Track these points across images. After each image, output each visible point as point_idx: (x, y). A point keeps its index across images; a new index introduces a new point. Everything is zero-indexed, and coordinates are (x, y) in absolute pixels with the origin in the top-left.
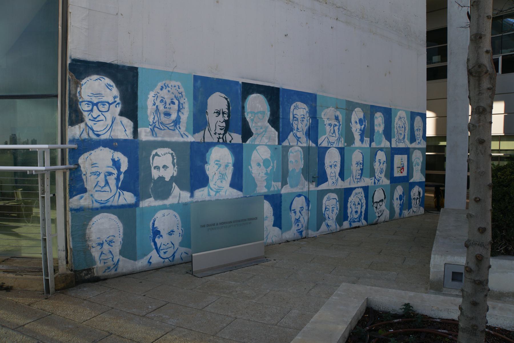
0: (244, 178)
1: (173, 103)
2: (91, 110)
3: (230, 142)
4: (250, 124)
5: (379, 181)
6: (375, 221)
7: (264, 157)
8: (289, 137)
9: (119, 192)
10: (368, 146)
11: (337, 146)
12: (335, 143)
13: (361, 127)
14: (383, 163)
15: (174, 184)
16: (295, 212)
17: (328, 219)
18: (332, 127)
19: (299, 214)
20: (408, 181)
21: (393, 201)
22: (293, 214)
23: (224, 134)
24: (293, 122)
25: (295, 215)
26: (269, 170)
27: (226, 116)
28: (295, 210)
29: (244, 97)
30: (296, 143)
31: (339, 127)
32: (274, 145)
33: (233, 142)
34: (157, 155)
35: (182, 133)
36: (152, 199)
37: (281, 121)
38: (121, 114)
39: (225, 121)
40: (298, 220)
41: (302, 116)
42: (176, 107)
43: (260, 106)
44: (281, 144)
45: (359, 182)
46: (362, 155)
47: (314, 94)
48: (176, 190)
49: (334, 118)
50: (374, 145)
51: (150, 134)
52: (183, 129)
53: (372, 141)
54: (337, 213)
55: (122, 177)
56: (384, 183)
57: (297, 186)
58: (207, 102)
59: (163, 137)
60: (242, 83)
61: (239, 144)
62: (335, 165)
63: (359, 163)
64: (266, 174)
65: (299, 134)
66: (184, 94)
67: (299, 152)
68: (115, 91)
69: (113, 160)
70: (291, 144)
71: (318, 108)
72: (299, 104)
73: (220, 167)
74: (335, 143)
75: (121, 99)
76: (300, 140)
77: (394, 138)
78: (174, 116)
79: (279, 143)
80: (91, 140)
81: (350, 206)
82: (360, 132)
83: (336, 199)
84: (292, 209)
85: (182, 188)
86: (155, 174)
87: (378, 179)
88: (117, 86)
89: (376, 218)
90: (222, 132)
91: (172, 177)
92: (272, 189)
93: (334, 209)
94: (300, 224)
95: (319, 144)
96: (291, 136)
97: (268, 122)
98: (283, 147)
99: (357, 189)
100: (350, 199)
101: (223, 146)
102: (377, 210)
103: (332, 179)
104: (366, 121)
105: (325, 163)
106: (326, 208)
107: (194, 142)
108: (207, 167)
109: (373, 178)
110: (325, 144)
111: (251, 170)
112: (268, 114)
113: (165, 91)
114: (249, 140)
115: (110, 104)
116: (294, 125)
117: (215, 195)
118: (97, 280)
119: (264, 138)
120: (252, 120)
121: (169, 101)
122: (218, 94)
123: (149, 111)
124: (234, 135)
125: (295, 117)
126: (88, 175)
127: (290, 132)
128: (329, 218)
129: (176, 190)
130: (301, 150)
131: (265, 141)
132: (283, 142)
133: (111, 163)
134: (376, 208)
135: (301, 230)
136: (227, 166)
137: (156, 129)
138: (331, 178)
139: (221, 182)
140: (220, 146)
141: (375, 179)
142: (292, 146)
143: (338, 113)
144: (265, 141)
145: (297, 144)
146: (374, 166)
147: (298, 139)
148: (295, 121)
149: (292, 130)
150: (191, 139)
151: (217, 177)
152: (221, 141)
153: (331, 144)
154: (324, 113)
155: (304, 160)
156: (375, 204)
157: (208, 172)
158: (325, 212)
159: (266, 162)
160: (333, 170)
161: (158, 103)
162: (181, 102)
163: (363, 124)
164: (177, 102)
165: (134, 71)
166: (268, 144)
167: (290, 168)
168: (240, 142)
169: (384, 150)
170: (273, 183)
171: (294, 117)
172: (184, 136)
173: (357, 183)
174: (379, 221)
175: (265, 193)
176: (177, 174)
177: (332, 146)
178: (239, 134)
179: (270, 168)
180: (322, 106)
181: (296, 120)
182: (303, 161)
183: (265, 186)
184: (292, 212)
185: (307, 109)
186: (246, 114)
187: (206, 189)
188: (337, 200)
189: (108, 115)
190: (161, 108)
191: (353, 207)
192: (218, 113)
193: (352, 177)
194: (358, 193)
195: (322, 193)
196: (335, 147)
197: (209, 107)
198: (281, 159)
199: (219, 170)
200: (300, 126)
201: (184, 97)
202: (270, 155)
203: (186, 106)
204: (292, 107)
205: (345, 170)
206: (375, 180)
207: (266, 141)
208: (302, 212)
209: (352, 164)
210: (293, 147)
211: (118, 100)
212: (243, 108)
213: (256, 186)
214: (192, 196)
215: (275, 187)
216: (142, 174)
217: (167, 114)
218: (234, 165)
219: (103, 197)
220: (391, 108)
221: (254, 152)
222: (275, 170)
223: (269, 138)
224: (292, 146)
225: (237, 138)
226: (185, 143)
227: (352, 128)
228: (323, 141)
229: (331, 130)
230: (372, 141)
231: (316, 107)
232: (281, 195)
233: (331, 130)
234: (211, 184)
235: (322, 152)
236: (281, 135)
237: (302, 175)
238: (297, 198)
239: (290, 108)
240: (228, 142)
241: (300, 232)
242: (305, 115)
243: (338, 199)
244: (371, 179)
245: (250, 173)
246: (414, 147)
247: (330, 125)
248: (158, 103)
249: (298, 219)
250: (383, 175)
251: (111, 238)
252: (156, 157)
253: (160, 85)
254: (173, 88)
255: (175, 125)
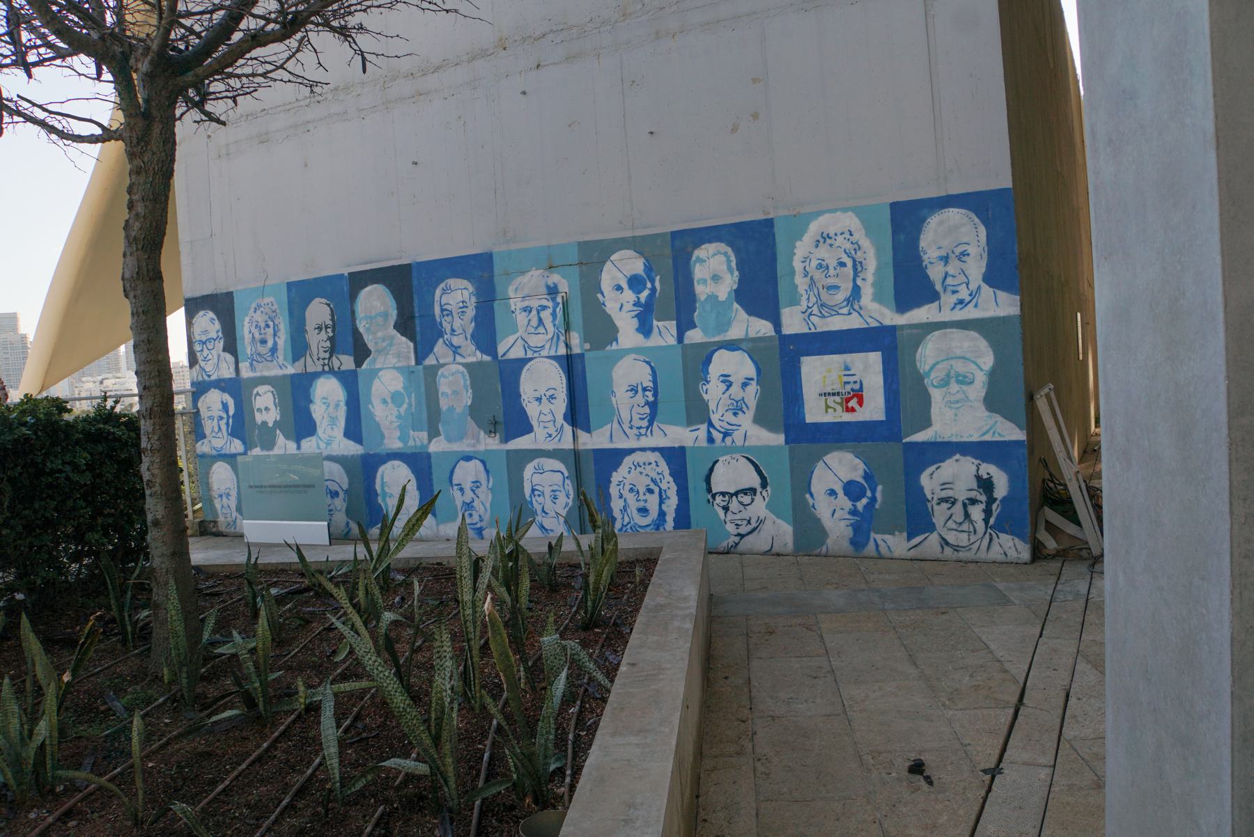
0: (363, 424)
1: (268, 326)
2: (202, 350)
3: (339, 368)
4: (365, 337)
5: (726, 434)
6: (724, 544)
7: (392, 389)
8: (436, 350)
9: (990, 534)
10: (672, 341)
11: (552, 353)
12: (547, 346)
13: (638, 298)
14: (745, 385)
15: (278, 431)
16: (462, 490)
17: (544, 514)
18: (534, 312)
19: (471, 494)
20: (897, 437)
21: (808, 496)
22: (457, 494)
23: (329, 359)
24: (443, 320)
25: (462, 495)
26: (402, 410)
27: (329, 330)
28: (460, 485)
29: (353, 296)
30: (452, 358)
31: (554, 311)
32: (409, 367)
33: (343, 368)
34: (258, 394)
35: (281, 363)
36: (258, 449)
37: (417, 321)
38: (224, 350)
39: (330, 339)
40: (469, 506)
41: (461, 305)
42: (271, 331)
43: (379, 305)
44: (421, 364)
45: (646, 435)
46: (649, 367)
47: (486, 253)
48: (281, 439)
49: (544, 290)
50: (695, 336)
51: (249, 369)
52: (281, 358)
53: (684, 324)
54: (567, 504)
55: (231, 420)
56: (751, 442)
57: (461, 438)
58: (304, 316)
59: (262, 371)
60: (349, 274)
61: (351, 371)
62: (552, 397)
63: (640, 389)
64: (399, 417)
65: (456, 341)
66: (278, 311)
67: (460, 375)
68: (217, 325)
69: (978, 478)
70: (441, 361)
71: (496, 279)
72: (452, 282)
73: (328, 406)
74: (547, 346)
75: (223, 333)
76: (459, 351)
77: (794, 301)
78: (270, 344)
79: (418, 362)
80: (204, 381)
81: (618, 494)
82: (635, 308)
83: (562, 473)
84: (455, 482)
85: (287, 437)
86: (259, 418)
87: (723, 430)
88: (218, 319)
89: (729, 538)
90: (327, 355)
91: (275, 422)
92: (411, 443)
93: (557, 493)
94: (474, 513)
95: (500, 355)
96: (439, 347)
97: (395, 327)
98: (425, 368)
99: (638, 452)
100: (616, 477)
101: (330, 375)
102: (730, 516)
103: (545, 427)
104: (658, 277)
105: (522, 394)
106: (533, 490)
107: (294, 374)
108: (312, 407)
109: (704, 427)
110: (517, 353)
111: (372, 410)
112: (394, 314)
113: (258, 312)
114: (366, 362)
115: (215, 340)
116: (444, 324)
117: (326, 448)
118: (219, 534)
119: (389, 356)
120: (368, 330)
121: (263, 325)
122: (317, 300)
123: (246, 342)
124: (344, 358)
125: (446, 310)
126: (206, 419)
127: (437, 340)
128: (543, 511)
129: (281, 439)
130: (465, 370)
131: (392, 361)
132: (424, 359)
133: (221, 407)
134: (726, 509)
135: (478, 526)
136: (337, 405)
137: (254, 362)
138: (542, 424)
139: (332, 429)
140: (327, 375)
141: (711, 430)
142: (443, 365)
143: (555, 278)
144: (392, 361)
145: (454, 360)
146: (704, 395)
147: (456, 350)
148: (445, 318)
149: (441, 334)
150: (291, 370)
151: (326, 422)
152: (327, 368)
153: (535, 352)
154: (515, 287)
155: (471, 388)
156: (719, 499)
157: (314, 416)
158: (531, 496)
159: (396, 398)
160: (546, 407)
161: (253, 330)
162: (276, 323)
163: (645, 288)
164: (271, 324)
165: (229, 296)
166: (396, 365)
167: (444, 404)
168: (353, 366)
169: (744, 346)
170: (411, 432)
171: (442, 310)
172: (283, 367)
173: (638, 439)
174: (741, 547)
175: (399, 448)
176: (281, 418)
177: (535, 355)
178: (351, 355)
179: (405, 406)
180: (508, 274)
181: (448, 315)
182: (470, 391)
183: (399, 438)
184: (455, 488)
185: (471, 289)
186: (357, 322)
187: (313, 439)
188: (566, 474)
189: (214, 352)
190: (257, 335)
191: (631, 498)
192: (320, 328)
193: (615, 422)
194: (644, 464)
195: (518, 460)
196: (546, 357)
197: (308, 322)
198: (423, 389)
199: (327, 412)
200: (457, 324)
201: (279, 315)
202: (402, 385)
203: (282, 327)
204: (438, 292)
205: (591, 409)
206: (709, 432)
207: (394, 361)
208: (478, 491)
209: (613, 391)
210: (446, 367)
211: (220, 334)
212: (353, 313)
213: (383, 436)
214: (299, 448)
215: (417, 439)
216: (247, 418)
217: (264, 342)
218: (347, 404)
219: (218, 443)
220: (770, 217)
221: (375, 382)
222: (413, 410)
223: (398, 355)
224: (443, 365)
225: (347, 362)
226: (284, 376)
227: (606, 303)
228: (509, 347)
229: (530, 320)
230: (684, 324)
231: (491, 277)
232: (429, 456)
233: (530, 320)
234: (320, 431)
235: (510, 372)
236: (419, 347)
237: (469, 418)
238: (462, 463)
239: (433, 295)
240: (336, 369)
241: (478, 529)
242: (468, 301)
243: (569, 473)
244: (693, 428)
245: (371, 416)
246: (925, 320)
247: (528, 310)
248: (253, 330)
249: (468, 502)
250: (746, 421)
251: (228, 490)
252: (258, 397)
253: (254, 305)
254: (266, 307)
255: (272, 355)
